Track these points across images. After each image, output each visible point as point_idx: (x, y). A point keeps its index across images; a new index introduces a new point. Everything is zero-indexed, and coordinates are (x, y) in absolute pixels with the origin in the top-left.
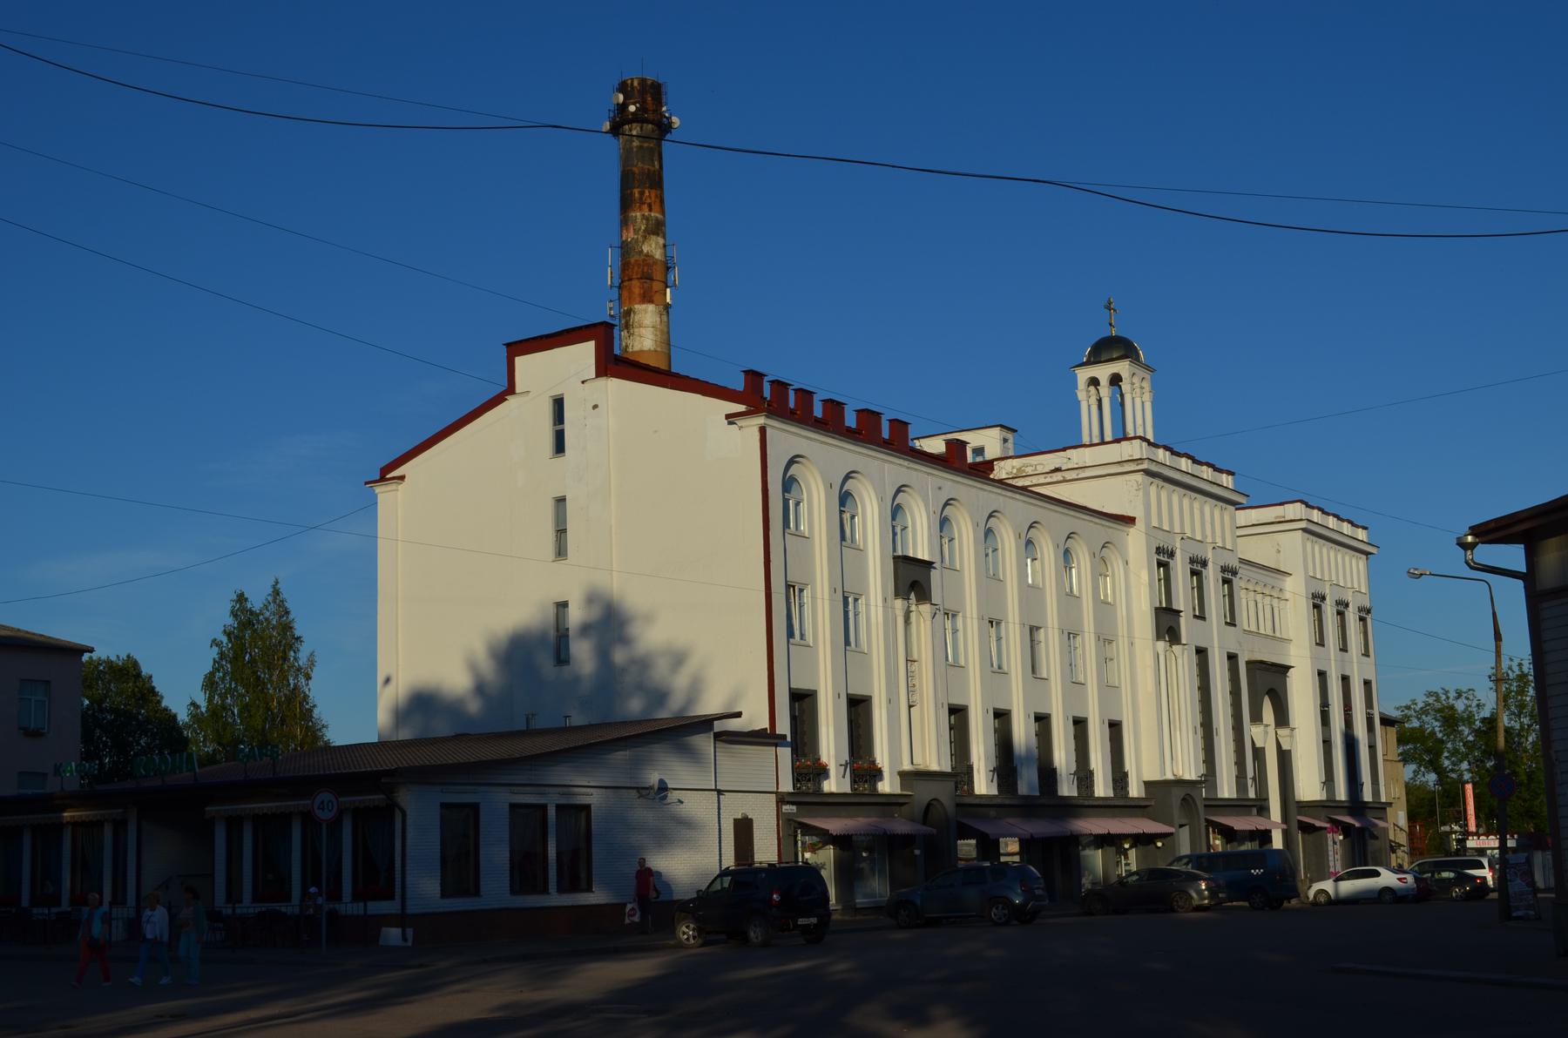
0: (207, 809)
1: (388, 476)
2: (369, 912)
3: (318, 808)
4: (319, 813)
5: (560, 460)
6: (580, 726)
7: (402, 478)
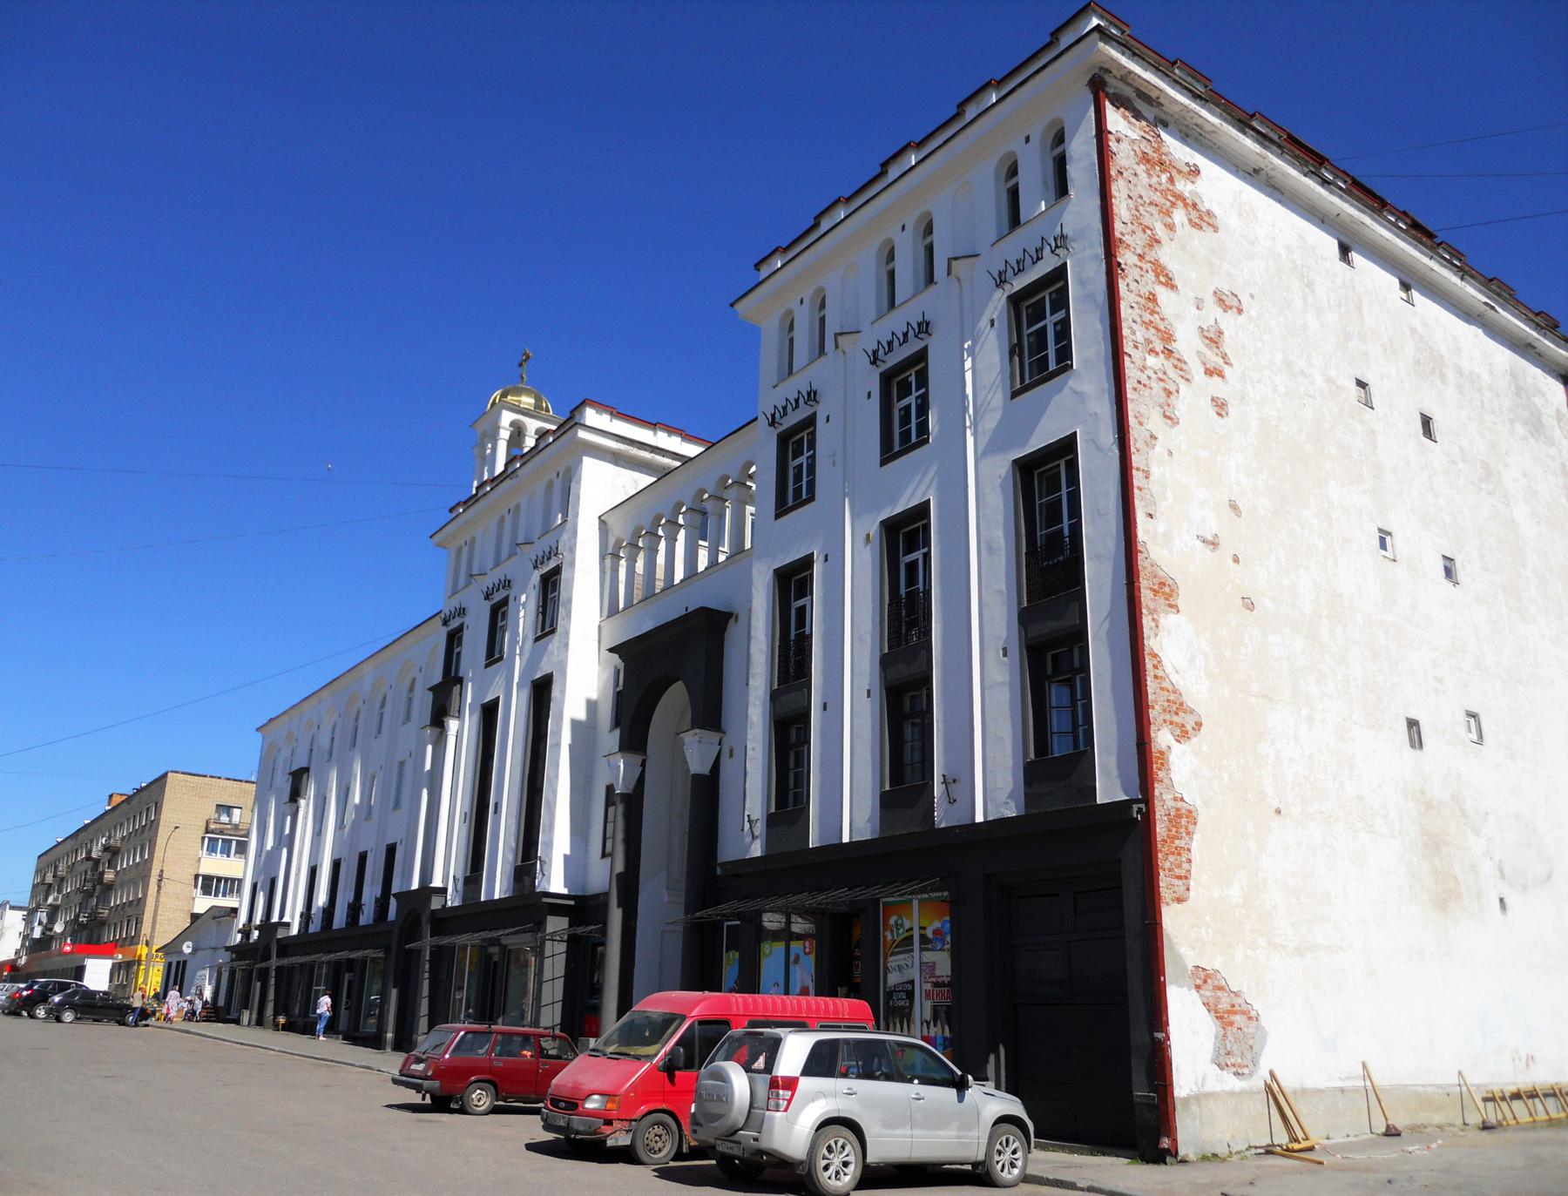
2: (766, 947)
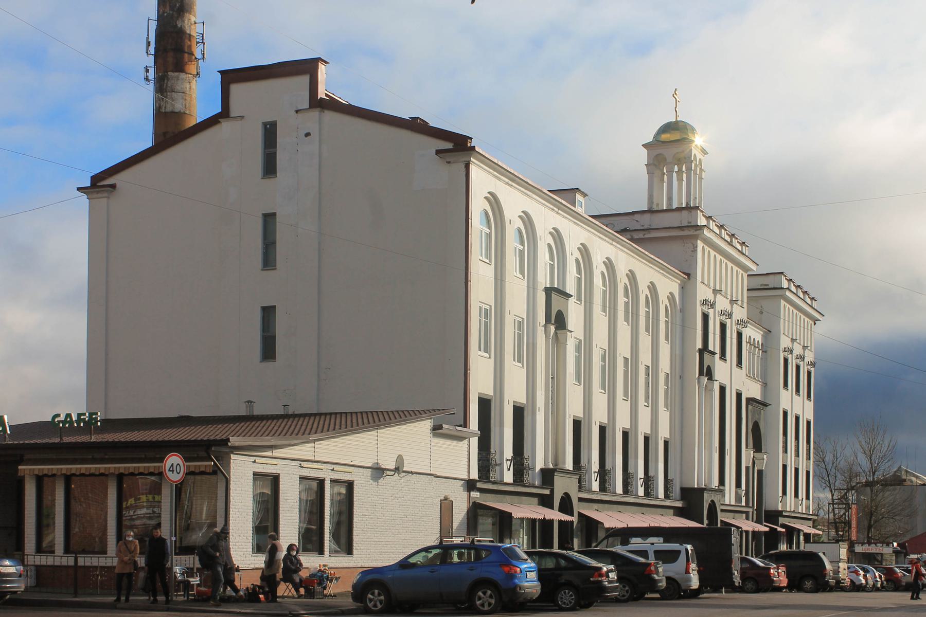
0: (20, 467)
1: (99, 184)
3: (169, 470)
4: (170, 474)
5: (269, 182)
6: (243, 416)
7: (113, 186)
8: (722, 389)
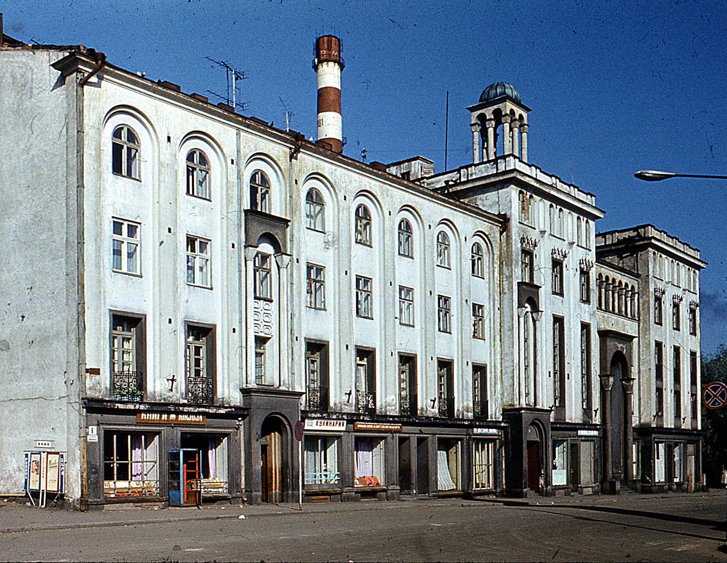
8: (558, 321)
